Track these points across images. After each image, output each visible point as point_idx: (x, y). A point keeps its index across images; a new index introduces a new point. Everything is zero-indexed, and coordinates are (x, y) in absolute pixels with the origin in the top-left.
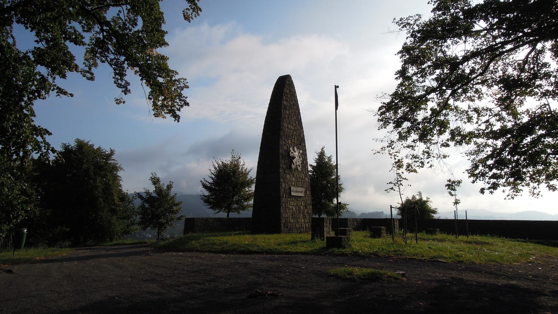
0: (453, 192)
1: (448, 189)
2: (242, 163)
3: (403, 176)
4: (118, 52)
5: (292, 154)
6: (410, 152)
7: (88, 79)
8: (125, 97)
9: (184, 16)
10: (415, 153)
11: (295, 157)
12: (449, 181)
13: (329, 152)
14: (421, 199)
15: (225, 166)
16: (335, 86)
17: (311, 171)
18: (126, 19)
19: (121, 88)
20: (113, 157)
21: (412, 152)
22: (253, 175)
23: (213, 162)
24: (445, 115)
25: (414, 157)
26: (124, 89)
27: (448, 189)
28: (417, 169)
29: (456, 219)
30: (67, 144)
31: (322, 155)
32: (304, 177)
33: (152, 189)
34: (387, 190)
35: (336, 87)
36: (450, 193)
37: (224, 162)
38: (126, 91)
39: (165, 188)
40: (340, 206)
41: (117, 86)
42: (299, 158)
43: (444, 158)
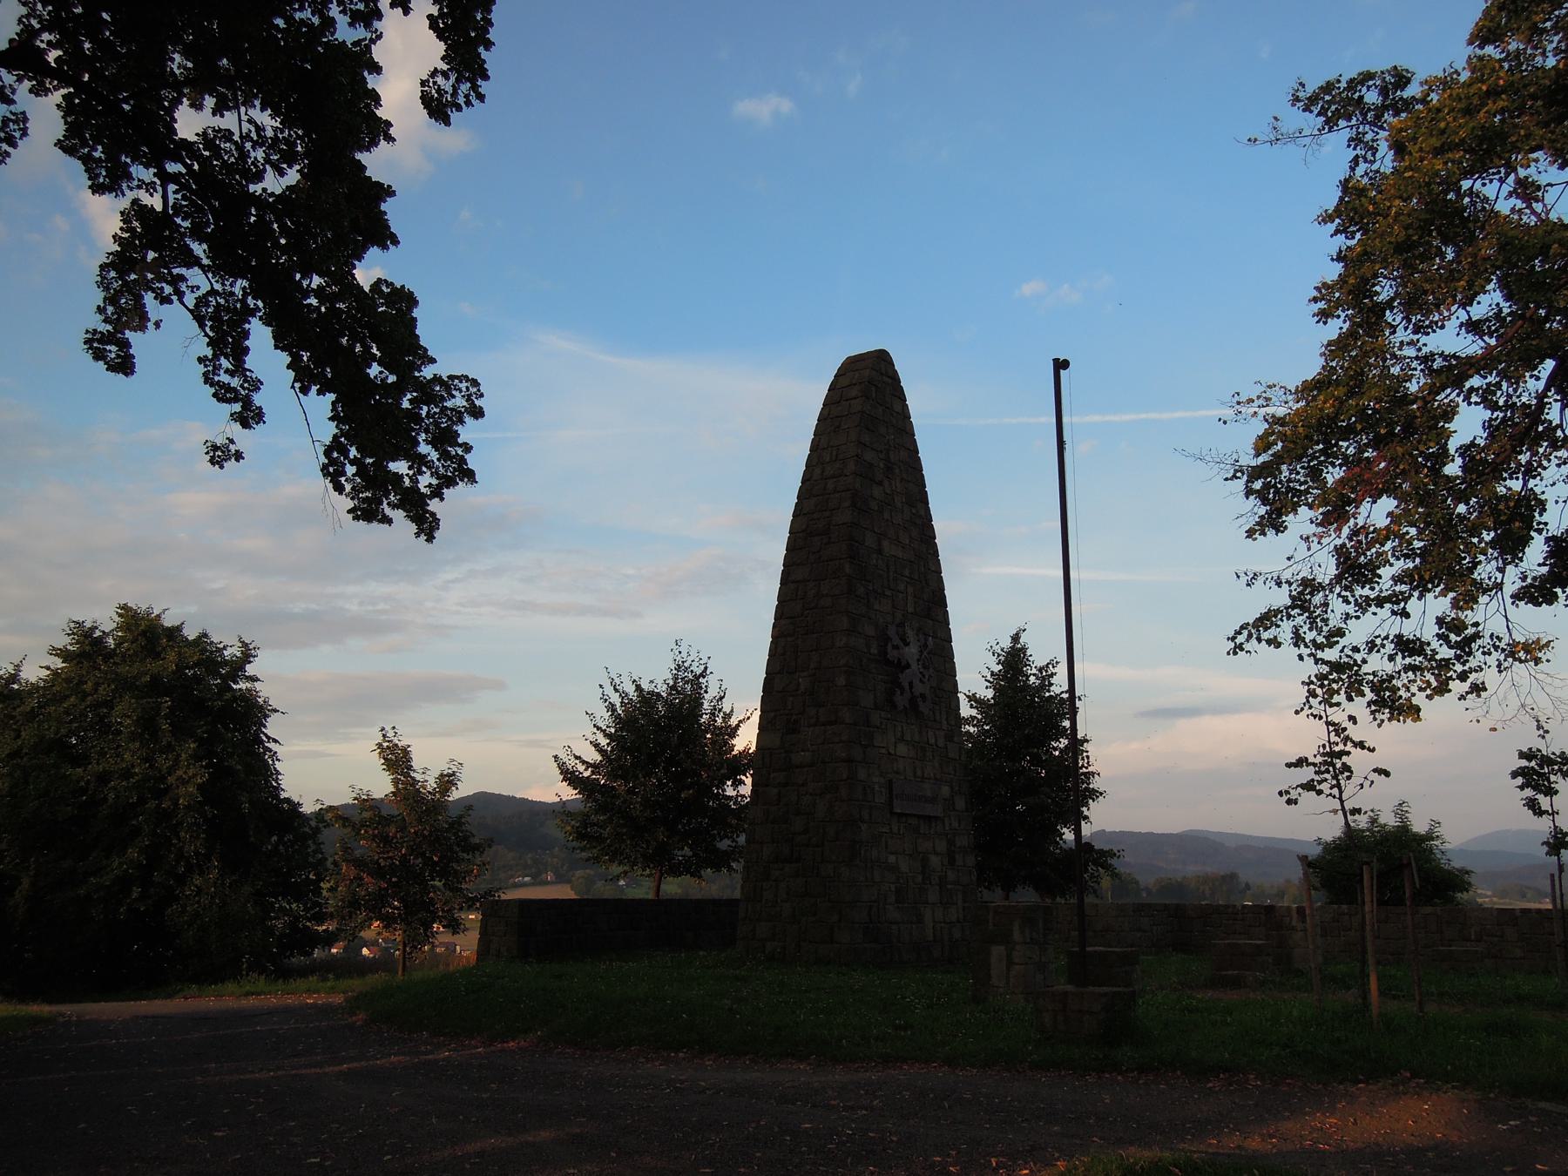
0: (1544, 802)
1: (1522, 788)
2: (713, 692)
3: (1354, 732)
4: (223, 265)
5: (895, 652)
6: (1386, 625)
7: (112, 368)
8: (244, 439)
9: (1017, 634)
10: (1408, 628)
11: (908, 666)
12: (1527, 755)
13: (1043, 649)
14: (1404, 829)
15: (647, 699)
16: (1056, 361)
17: (973, 718)
18: (245, 131)
19: (228, 401)
20: (250, 669)
21: (1395, 626)
22: (746, 739)
23: (601, 686)
24: (1530, 472)
25: (1406, 646)
26: (237, 407)
27: (1522, 788)
28: (1419, 699)
29: (1559, 906)
30: (88, 625)
31: (1014, 659)
32: (941, 743)
33: (381, 785)
34: (1287, 792)
35: (1060, 365)
36: (1532, 805)
37: (645, 686)
38: (249, 416)
39: (432, 784)
40: (1091, 856)
41: (215, 395)
42: (924, 668)
43: (1371, 712)
